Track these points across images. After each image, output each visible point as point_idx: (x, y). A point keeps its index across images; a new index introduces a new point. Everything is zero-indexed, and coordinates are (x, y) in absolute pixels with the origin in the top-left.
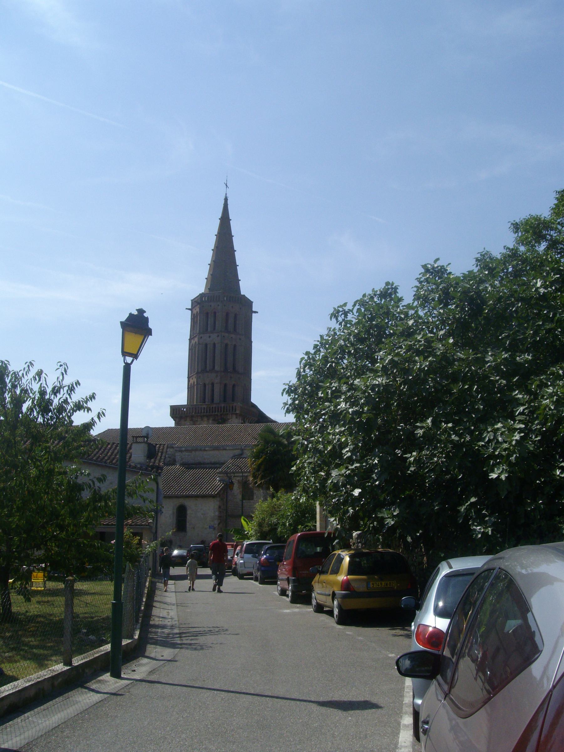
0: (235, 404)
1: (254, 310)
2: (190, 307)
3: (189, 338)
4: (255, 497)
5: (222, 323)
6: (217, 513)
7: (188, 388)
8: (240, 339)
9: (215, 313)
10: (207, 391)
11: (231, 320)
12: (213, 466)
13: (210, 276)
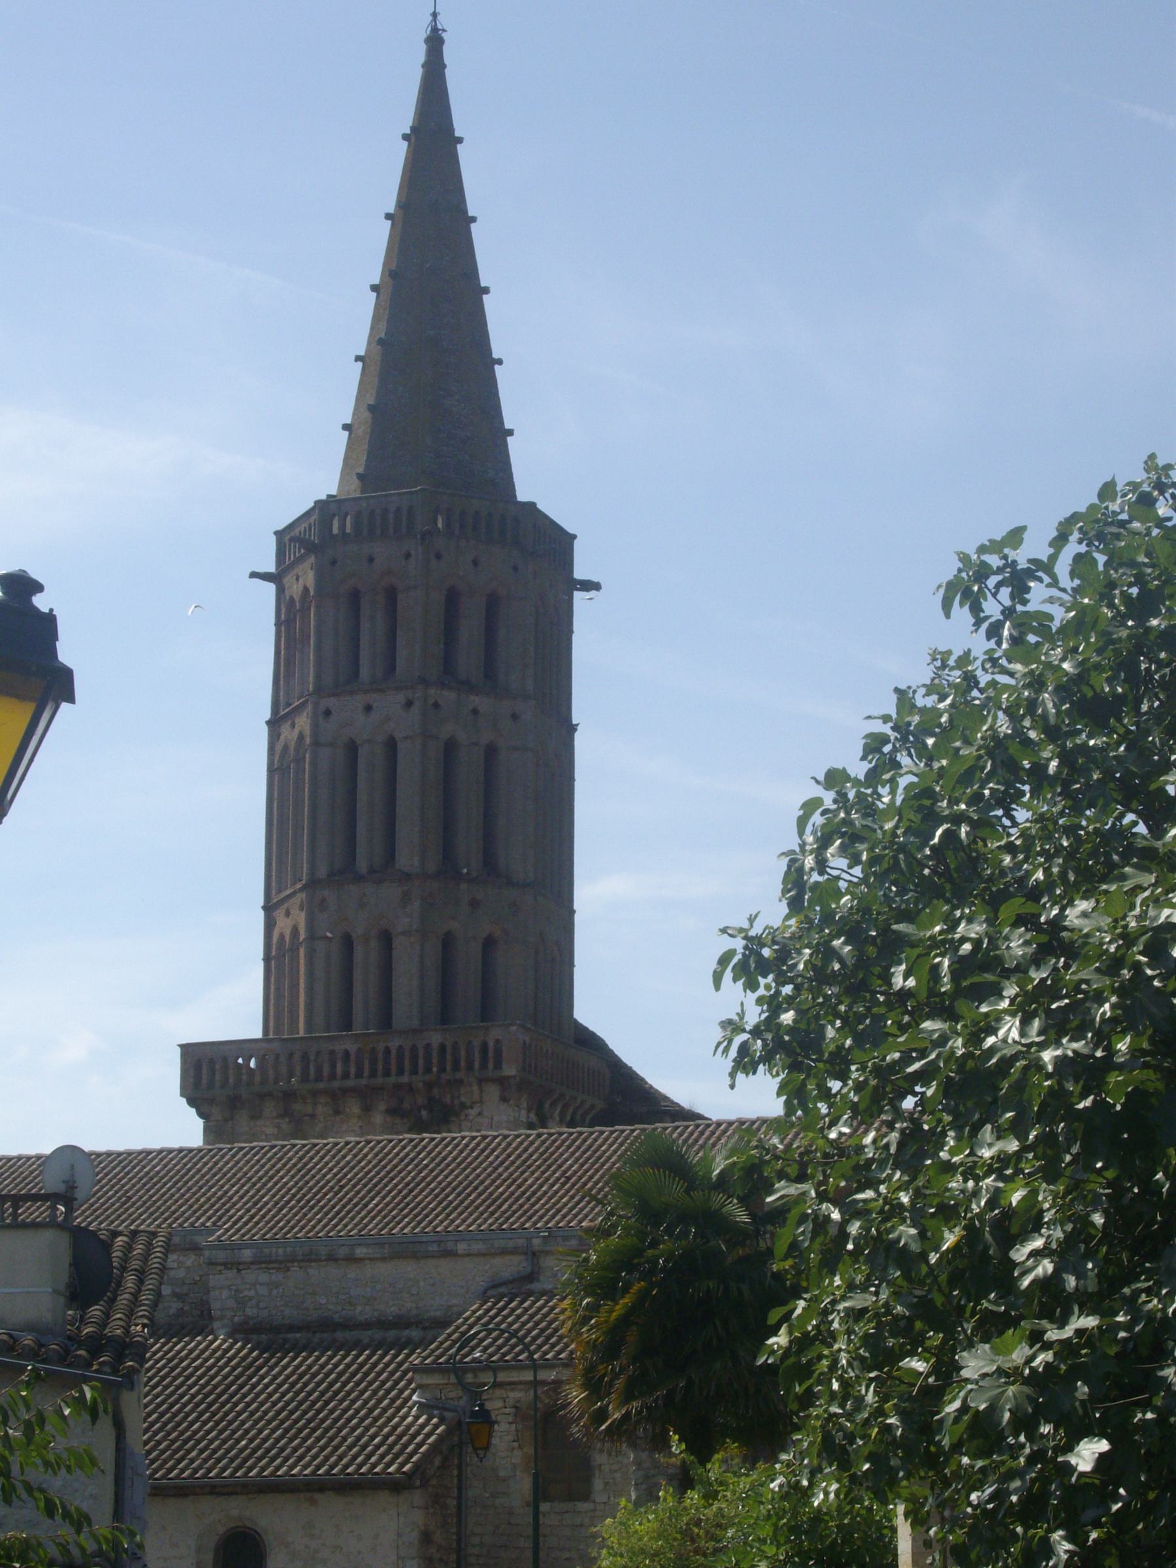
0: (495, 1033)
1: (579, 573)
2: (271, 567)
4: (598, 1484)
7: (267, 959)
8: (515, 717)
9: (392, 596)
11: (470, 628)
13: (366, 415)
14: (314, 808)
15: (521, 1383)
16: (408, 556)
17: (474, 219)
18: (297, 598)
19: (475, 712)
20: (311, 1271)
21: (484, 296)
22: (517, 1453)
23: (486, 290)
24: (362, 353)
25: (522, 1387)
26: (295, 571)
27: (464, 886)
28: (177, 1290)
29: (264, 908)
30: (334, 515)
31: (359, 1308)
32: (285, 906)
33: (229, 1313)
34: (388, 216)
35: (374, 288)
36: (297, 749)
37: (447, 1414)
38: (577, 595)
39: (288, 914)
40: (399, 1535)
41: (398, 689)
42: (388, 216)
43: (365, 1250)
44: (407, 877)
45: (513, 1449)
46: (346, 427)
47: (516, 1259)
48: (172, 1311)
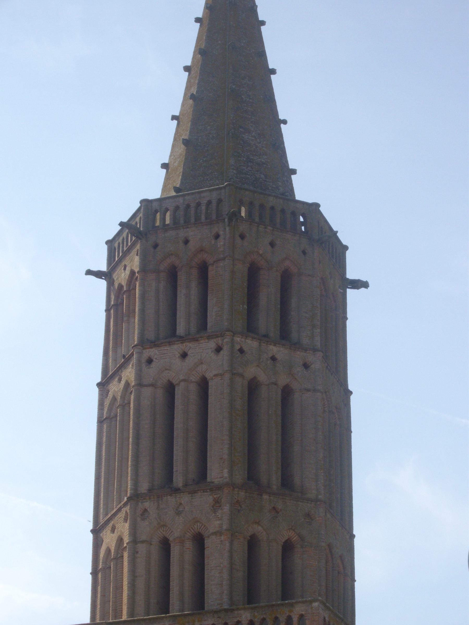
0: (299, 609)
1: (351, 274)
2: (103, 267)
3: (91, 526)
7: (94, 573)
8: (306, 366)
9: (203, 270)
11: (268, 295)
13: (182, 148)
16: (217, 236)
17: (263, 23)
18: (124, 283)
19: (273, 359)
21: (272, 76)
23: (273, 72)
24: (177, 114)
26: (123, 264)
27: (265, 497)
29: (93, 531)
30: (156, 211)
32: (111, 524)
34: (198, 20)
35: (187, 69)
36: (123, 397)
38: (350, 292)
39: (113, 530)
41: (209, 338)
42: (198, 20)
44: (219, 488)
46: (164, 166)
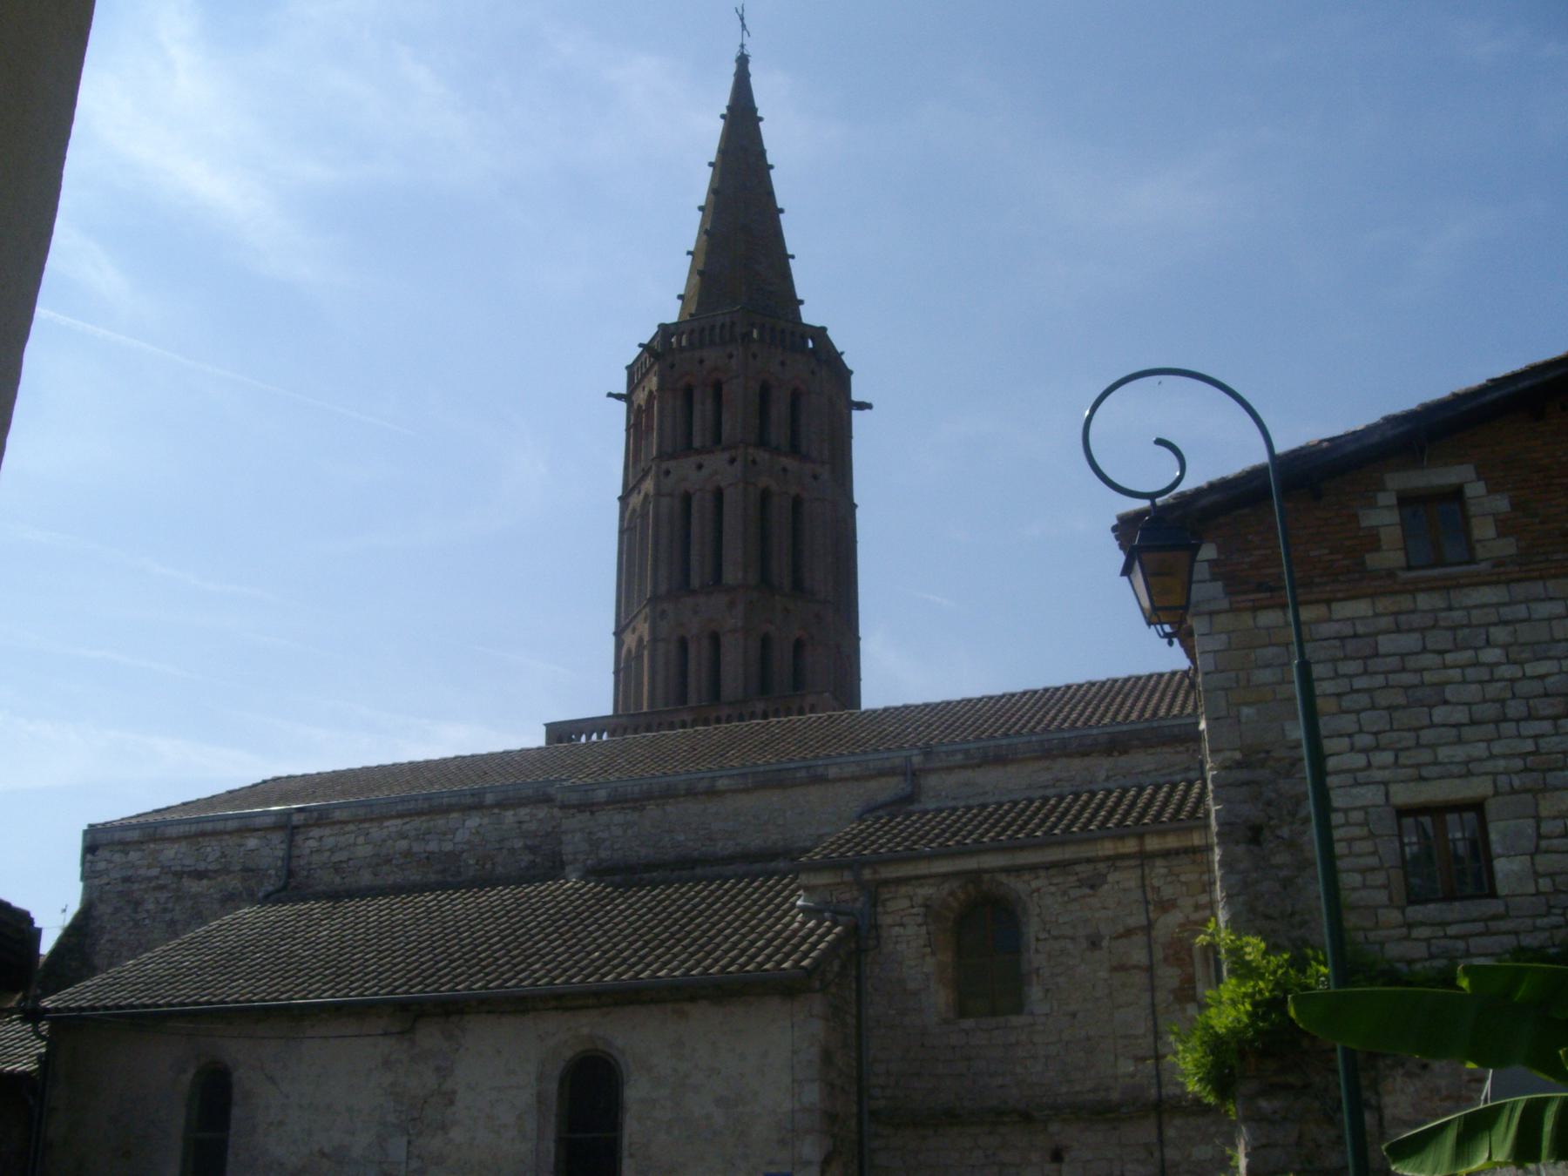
2: (623, 390)
4: (1035, 992)
5: (740, 428)
6: (812, 1094)
7: (617, 673)
8: (815, 477)
9: (718, 388)
10: (692, 666)
12: (757, 867)
13: (697, 279)
14: (656, 543)
15: (931, 876)
19: (785, 470)
20: (669, 808)
22: (930, 960)
25: (931, 881)
28: (529, 843)
31: (720, 844)
33: (581, 857)
34: (711, 164)
37: (840, 918)
40: (794, 1052)
41: (724, 450)
42: (711, 164)
43: (726, 781)
45: (924, 956)
46: (680, 297)
47: (894, 781)
48: (523, 865)
